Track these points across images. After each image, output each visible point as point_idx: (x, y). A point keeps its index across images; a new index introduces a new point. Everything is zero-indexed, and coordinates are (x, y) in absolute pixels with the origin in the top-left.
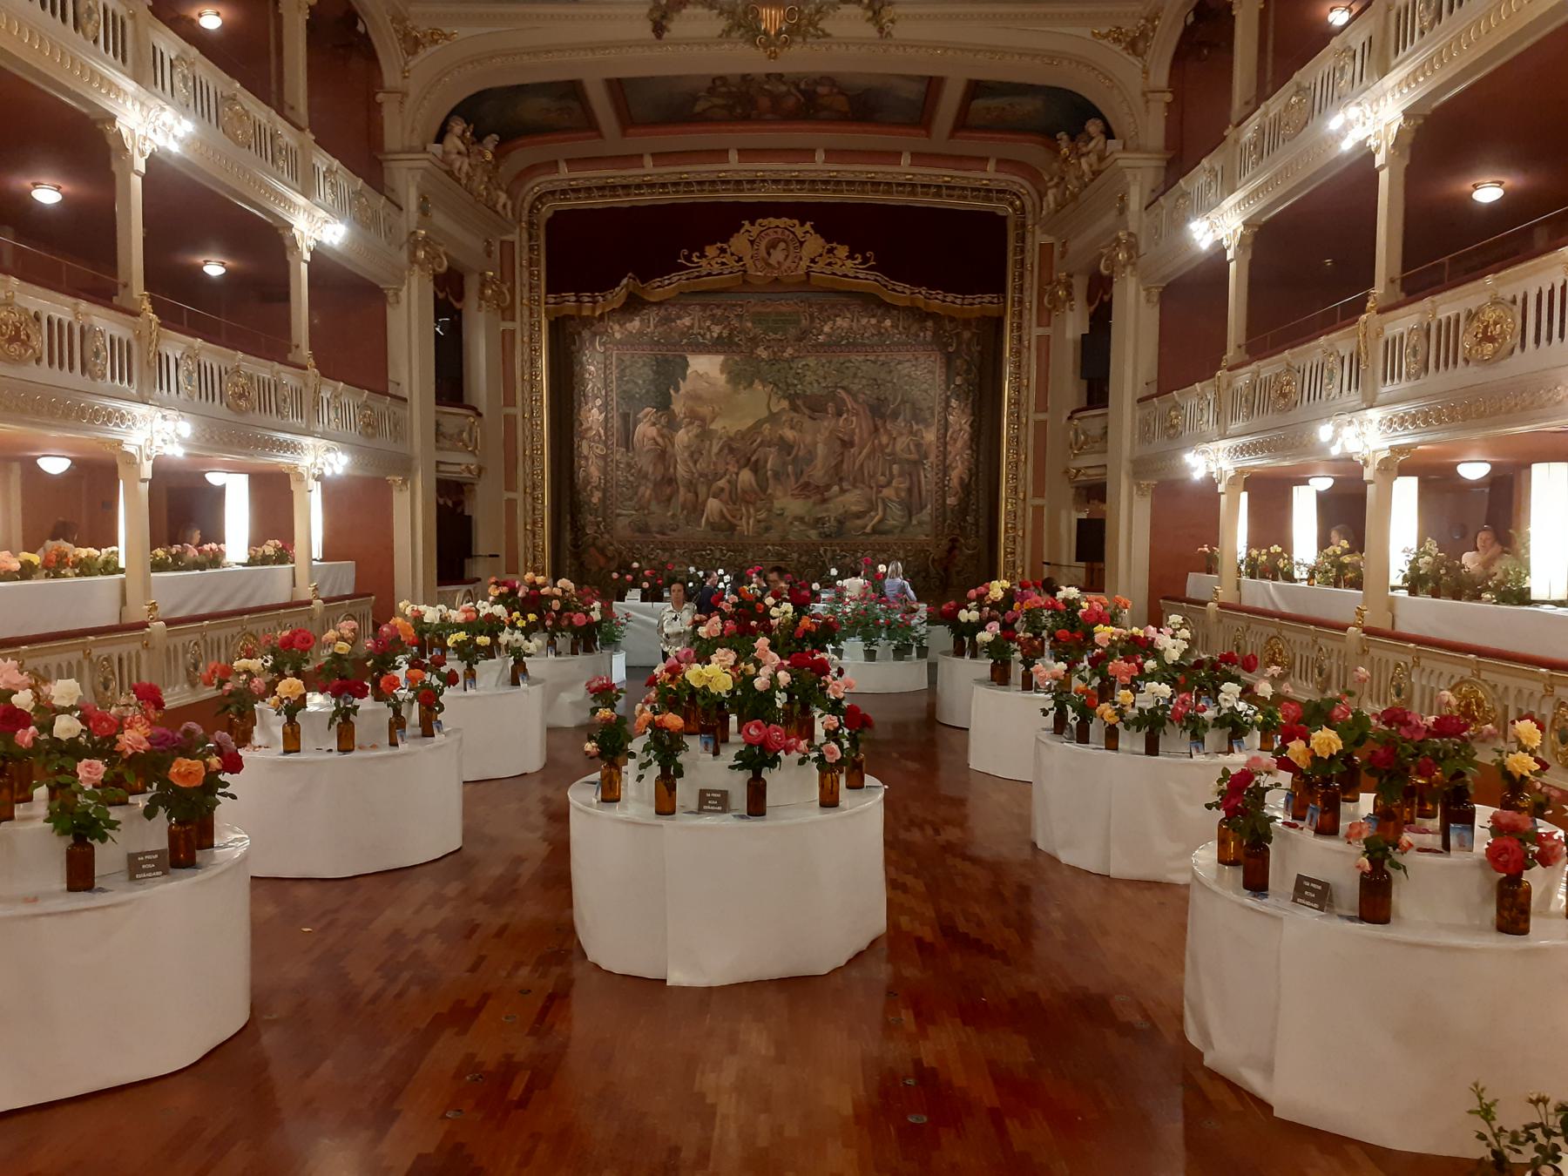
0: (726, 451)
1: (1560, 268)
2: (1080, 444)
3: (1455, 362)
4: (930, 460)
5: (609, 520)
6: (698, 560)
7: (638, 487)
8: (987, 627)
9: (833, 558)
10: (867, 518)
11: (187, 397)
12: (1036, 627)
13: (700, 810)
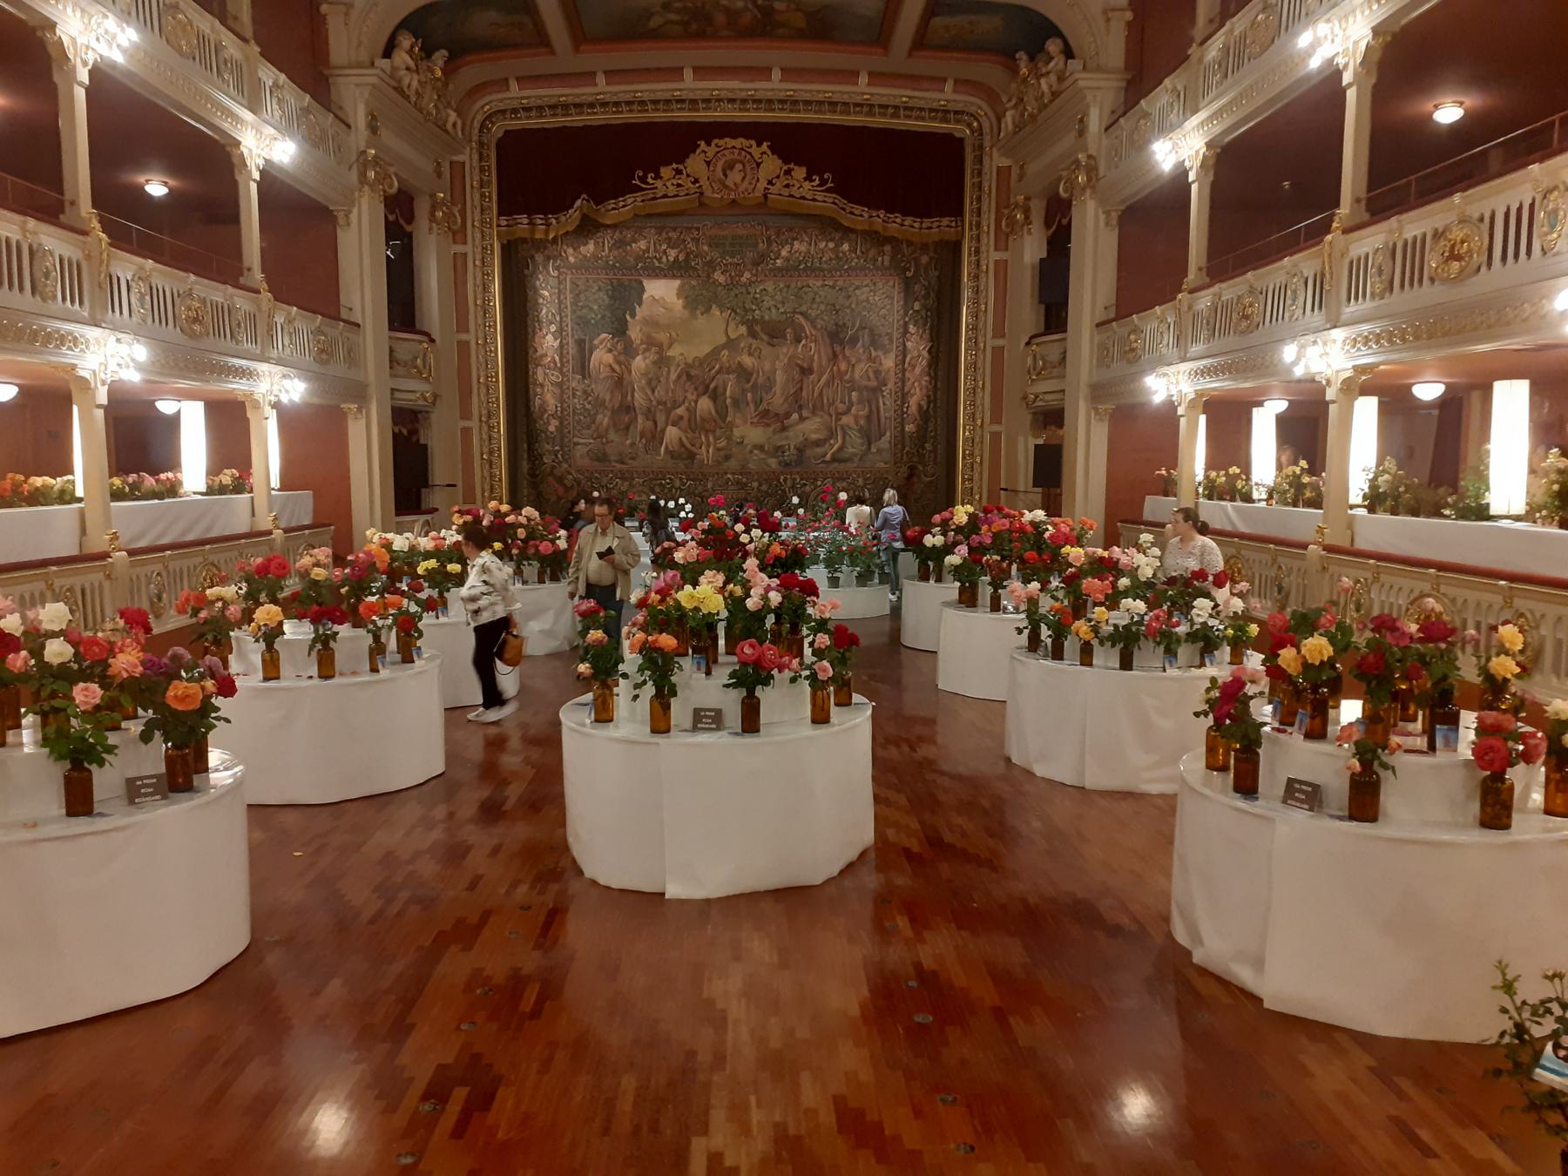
0: (684, 377)
1: (1528, 186)
2: (1038, 369)
3: (1421, 281)
4: (889, 387)
5: (566, 449)
6: (657, 489)
7: (596, 415)
8: (956, 550)
9: (793, 487)
10: (827, 445)
11: (140, 321)
12: (1004, 550)
13: (695, 728)
